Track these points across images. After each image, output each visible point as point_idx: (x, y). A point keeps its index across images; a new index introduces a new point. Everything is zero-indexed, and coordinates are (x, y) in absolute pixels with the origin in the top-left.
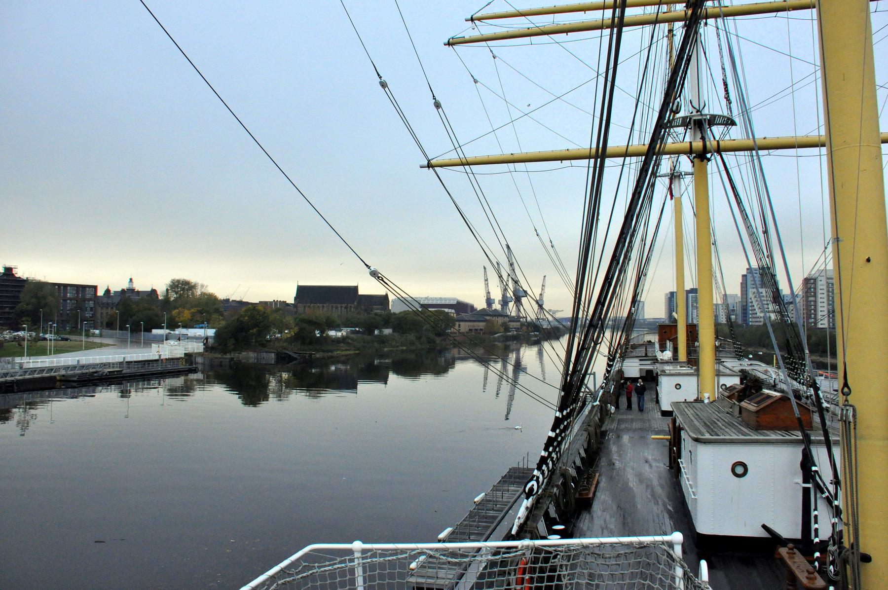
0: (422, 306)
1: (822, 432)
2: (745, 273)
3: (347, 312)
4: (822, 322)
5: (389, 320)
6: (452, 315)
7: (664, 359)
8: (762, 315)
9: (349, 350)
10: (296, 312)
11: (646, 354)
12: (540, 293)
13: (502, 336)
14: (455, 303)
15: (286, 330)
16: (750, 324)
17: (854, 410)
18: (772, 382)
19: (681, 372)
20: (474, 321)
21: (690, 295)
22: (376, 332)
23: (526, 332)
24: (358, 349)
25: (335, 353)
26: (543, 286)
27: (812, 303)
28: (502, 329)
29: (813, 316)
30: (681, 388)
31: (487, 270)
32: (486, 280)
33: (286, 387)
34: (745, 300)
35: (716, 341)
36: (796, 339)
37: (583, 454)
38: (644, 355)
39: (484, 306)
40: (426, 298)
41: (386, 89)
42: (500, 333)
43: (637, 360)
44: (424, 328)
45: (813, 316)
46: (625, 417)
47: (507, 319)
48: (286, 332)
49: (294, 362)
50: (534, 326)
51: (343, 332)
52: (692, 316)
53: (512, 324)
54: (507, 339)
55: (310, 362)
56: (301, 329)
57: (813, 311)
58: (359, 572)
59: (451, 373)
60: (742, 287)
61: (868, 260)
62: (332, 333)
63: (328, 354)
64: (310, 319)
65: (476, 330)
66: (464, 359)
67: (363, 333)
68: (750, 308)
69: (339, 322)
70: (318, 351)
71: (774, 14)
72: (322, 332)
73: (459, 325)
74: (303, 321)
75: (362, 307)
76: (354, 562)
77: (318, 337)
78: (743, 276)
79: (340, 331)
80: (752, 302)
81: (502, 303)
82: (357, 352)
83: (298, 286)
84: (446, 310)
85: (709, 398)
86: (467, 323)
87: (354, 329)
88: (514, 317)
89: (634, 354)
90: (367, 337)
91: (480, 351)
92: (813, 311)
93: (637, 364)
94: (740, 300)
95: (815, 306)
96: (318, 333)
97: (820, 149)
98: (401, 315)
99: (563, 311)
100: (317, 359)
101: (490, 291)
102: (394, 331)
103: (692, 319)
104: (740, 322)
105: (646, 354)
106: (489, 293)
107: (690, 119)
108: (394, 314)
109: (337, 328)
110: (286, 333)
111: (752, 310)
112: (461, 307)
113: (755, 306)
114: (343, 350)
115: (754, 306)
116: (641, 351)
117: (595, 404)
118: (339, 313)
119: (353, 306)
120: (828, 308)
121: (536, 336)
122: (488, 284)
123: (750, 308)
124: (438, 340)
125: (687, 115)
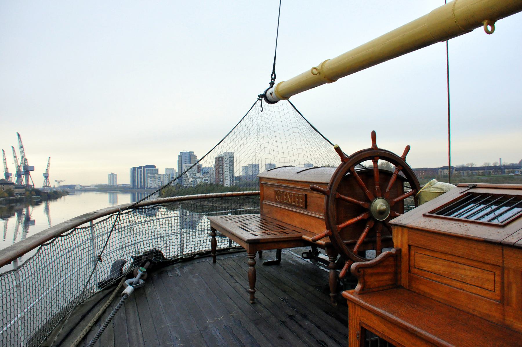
1: (282, 257)
2: (179, 155)
4: (226, 183)
12: (46, 169)
13: (5, 199)
21: (146, 169)
23: (29, 196)
26: (48, 164)
27: (221, 172)
28: (6, 194)
29: (221, 180)
31: (5, 152)
32: (5, 159)
42: (4, 197)
50: (38, 192)
52: (147, 182)
53: (17, 190)
54: (9, 202)
76: (368, 342)
81: (17, 176)
95: (223, 174)
99: (65, 181)
101: (8, 167)
103: (147, 184)
106: (7, 168)
120: (230, 175)
121: (38, 198)
122: (6, 162)
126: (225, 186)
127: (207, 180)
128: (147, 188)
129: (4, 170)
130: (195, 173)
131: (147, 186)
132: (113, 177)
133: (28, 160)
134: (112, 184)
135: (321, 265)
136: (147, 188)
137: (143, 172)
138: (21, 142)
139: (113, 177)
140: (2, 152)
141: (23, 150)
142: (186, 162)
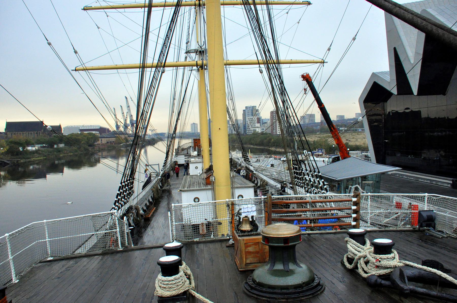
0: (81, 130)
2: (245, 109)
3: (38, 136)
5: (62, 139)
6: (97, 134)
7: (194, 155)
8: (252, 129)
9: (40, 157)
10: (6, 137)
11: (187, 153)
14: (99, 128)
15: (1, 148)
17: (215, 178)
18: (240, 163)
19: (198, 161)
20: (109, 137)
22: (55, 146)
24: (45, 156)
25: (32, 159)
29: (275, 129)
31: (116, 110)
33: (4, 180)
34: (244, 122)
35: (210, 147)
36: (383, 111)
37: (151, 200)
38: (186, 153)
39: (115, 129)
40: (83, 126)
41: (51, 46)
43: (183, 156)
44: (82, 142)
45: (275, 129)
46: (174, 183)
47: (126, 136)
48: (1, 149)
49: (8, 166)
51: (36, 147)
55: (18, 165)
56: (10, 147)
57: (275, 127)
59: (99, 165)
61: (220, 129)
62: (30, 148)
63: (28, 160)
64: (16, 141)
65: (111, 142)
66: (105, 157)
67: (48, 147)
69: (33, 141)
70: (22, 159)
71: (233, 6)
72: (24, 148)
73: (101, 140)
74: (11, 142)
75: (46, 133)
77: (21, 151)
78: (244, 110)
79: (34, 147)
80: (248, 123)
81: (124, 127)
82: (44, 158)
83: (7, 122)
84: (94, 132)
85: (200, 173)
86: (106, 139)
87: (42, 145)
88: (131, 134)
89: (182, 153)
90: (51, 149)
91: (114, 153)
92: (275, 127)
93: (184, 158)
94: (242, 122)
96: (21, 149)
98: (69, 136)
100: (22, 163)
102: (65, 145)
105: (187, 153)
107: (197, 50)
108: (65, 136)
109: (32, 145)
110: (2, 150)
112: (102, 130)
114: (36, 157)
116: (185, 152)
117: (159, 178)
118: (33, 136)
119: (41, 132)
124: (90, 149)
125: (196, 48)
126: (316, 121)
127: (264, 129)
129: (115, 123)
130: (255, 124)
132: (194, 126)
133: (133, 116)
134: (193, 132)
135: (238, 263)
138: (128, 104)
139: (194, 126)
140: (120, 107)
141: (129, 109)
142: (249, 115)
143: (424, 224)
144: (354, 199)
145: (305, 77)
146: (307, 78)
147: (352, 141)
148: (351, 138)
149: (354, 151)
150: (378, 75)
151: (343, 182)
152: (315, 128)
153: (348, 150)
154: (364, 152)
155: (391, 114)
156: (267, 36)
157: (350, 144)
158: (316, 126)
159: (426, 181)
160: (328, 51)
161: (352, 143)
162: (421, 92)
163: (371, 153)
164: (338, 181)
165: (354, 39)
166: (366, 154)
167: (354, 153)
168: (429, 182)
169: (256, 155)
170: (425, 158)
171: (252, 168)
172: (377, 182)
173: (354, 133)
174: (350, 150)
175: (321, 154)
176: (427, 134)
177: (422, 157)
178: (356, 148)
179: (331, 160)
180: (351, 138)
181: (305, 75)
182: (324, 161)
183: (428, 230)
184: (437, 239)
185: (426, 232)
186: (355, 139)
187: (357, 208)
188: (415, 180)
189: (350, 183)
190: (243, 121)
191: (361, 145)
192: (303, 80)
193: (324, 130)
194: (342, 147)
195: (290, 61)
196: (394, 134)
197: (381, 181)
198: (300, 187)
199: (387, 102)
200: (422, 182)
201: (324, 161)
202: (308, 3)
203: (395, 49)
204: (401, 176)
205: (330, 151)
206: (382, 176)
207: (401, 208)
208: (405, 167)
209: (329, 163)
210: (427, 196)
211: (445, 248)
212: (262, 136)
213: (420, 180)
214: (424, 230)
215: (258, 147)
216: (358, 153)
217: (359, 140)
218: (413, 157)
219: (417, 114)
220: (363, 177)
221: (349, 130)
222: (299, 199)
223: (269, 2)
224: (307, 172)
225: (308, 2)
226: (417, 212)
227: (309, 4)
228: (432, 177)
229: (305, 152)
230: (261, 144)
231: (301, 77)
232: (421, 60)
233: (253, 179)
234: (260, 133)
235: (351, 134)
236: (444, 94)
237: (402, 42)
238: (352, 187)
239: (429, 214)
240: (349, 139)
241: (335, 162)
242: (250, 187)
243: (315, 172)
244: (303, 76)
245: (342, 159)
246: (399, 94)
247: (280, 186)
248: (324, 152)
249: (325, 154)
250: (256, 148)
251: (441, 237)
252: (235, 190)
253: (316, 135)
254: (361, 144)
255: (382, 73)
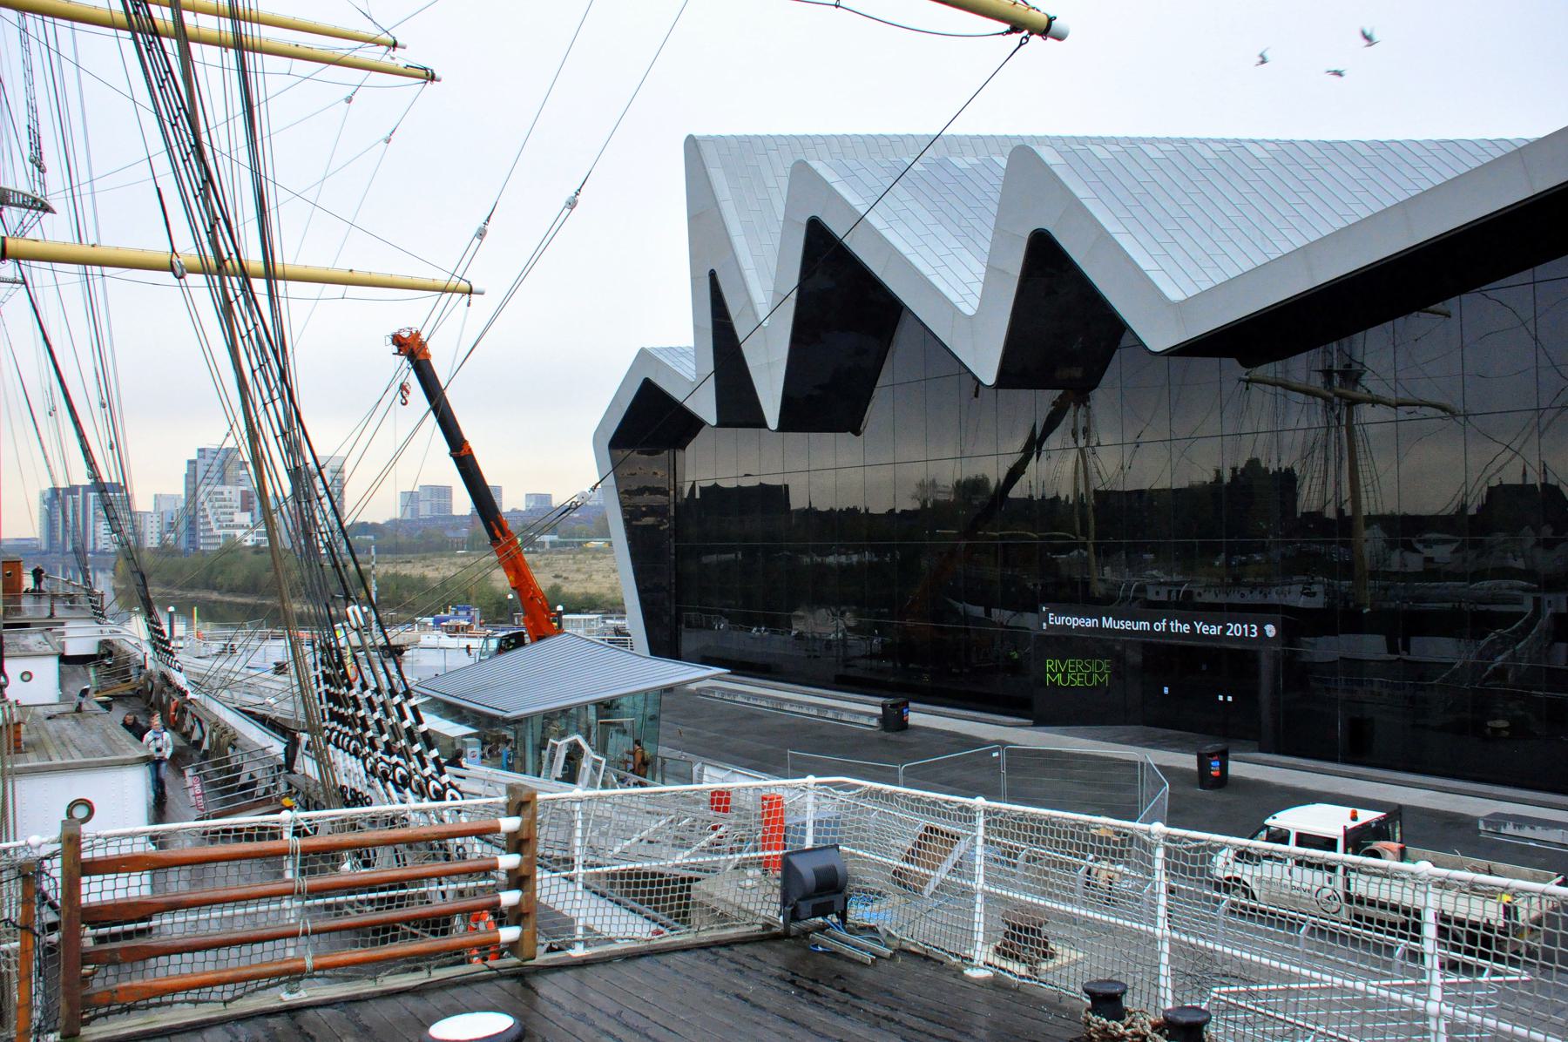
2: (194, 457)
8: (221, 532)
16: (202, 548)
18: (140, 657)
30: (19, 677)
58: (810, 825)
60: (187, 483)
68: (201, 520)
78: (190, 462)
80: (204, 510)
97: (1525, 480)
103: (95, 539)
104: (183, 544)
111: (203, 524)
113: (210, 517)
115: (207, 516)
123: (201, 520)
128: (94, 552)
130: (232, 514)
131: (95, 548)
136: (94, 552)
137: (81, 503)
143: (805, 907)
144: (510, 824)
145: (403, 342)
146: (411, 349)
147: (573, 581)
148: (572, 571)
149: (579, 613)
150: (660, 357)
151: (530, 724)
152: (450, 534)
153: (560, 612)
154: (611, 618)
155: (698, 496)
156: (270, 176)
157: (569, 589)
158: (456, 528)
159: (805, 711)
160: (477, 241)
161: (574, 587)
162: (790, 421)
163: (634, 621)
164: (517, 721)
165: (572, 204)
166: (618, 622)
167: (578, 621)
168: (814, 712)
169: (226, 627)
170: (800, 636)
171: (180, 679)
172: (653, 718)
173: (581, 553)
174: (567, 611)
175: (467, 623)
176: (806, 560)
177: (794, 633)
178: (587, 604)
179: (493, 644)
180: (572, 571)
181: (406, 335)
182: (468, 648)
183: (822, 929)
184: (851, 968)
185: (813, 940)
186: (586, 573)
187: (520, 865)
188: (773, 709)
189: (559, 725)
190: (187, 503)
191: (603, 595)
192: (399, 354)
193: (480, 543)
194: (532, 598)
195: (347, 275)
196: (706, 559)
197: (662, 715)
198: (351, 754)
199: (683, 448)
200: (792, 712)
201: (468, 648)
202: (427, 74)
203: (713, 274)
204: (729, 695)
205: (496, 612)
206: (664, 698)
207: (726, 810)
208: (742, 667)
209: (487, 657)
210: (812, 787)
211: (892, 1020)
212: (257, 557)
213: (787, 708)
214: (805, 933)
215: (239, 600)
216: (592, 620)
217: (597, 577)
218: (765, 631)
219: (774, 496)
220: (601, 703)
221: (566, 544)
222: (249, 838)
223: (241, 11)
224: (368, 693)
225: (426, 69)
226: (776, 856)
227: (431, 77)
228: (804, 693)
229: (354, 613)
230: (251, 587)
231: (389, 341)
232: (795, 291)
233: (188, 721)
234: (250, 547)
235: (571, 556)
236: (857, 432)
237: (734, 254)
238: (559, 743)
239: (821, 861)
240: (565, 575)
241: (507, 650)
242: (124, 764)
243: (393, 693)
244: (397, 340)
245: (532, 642)
246: (722, 423)
247: (282, 751)
248: (477, 616)
249: (481, 625)
250: (230, 603)
251: (868, 958)
252: (17, 784)
253: (454, 560)
254: (604, 591)
255: (670, 350)
